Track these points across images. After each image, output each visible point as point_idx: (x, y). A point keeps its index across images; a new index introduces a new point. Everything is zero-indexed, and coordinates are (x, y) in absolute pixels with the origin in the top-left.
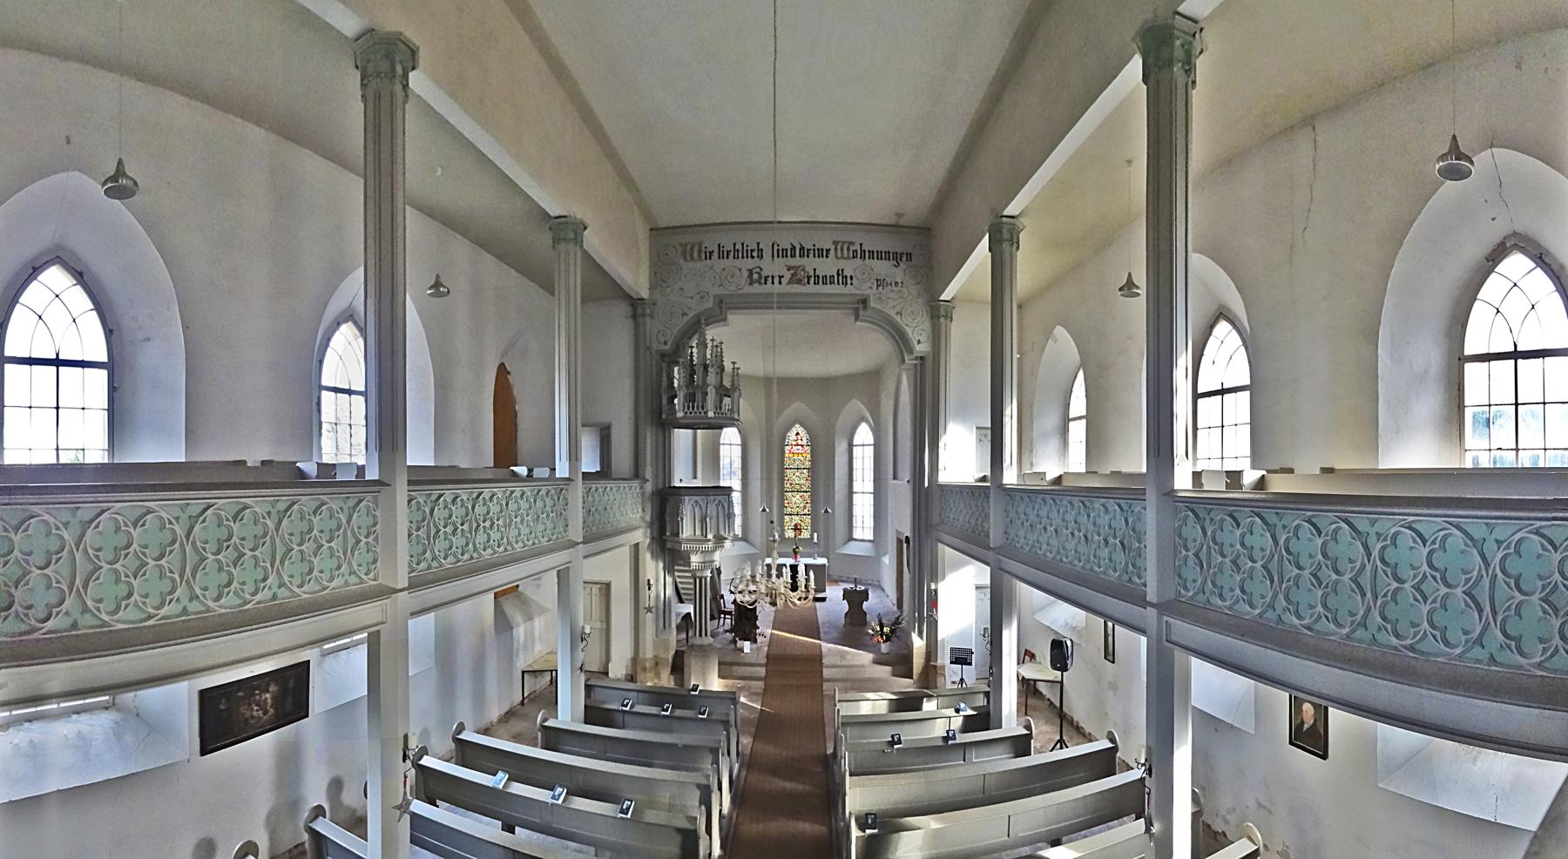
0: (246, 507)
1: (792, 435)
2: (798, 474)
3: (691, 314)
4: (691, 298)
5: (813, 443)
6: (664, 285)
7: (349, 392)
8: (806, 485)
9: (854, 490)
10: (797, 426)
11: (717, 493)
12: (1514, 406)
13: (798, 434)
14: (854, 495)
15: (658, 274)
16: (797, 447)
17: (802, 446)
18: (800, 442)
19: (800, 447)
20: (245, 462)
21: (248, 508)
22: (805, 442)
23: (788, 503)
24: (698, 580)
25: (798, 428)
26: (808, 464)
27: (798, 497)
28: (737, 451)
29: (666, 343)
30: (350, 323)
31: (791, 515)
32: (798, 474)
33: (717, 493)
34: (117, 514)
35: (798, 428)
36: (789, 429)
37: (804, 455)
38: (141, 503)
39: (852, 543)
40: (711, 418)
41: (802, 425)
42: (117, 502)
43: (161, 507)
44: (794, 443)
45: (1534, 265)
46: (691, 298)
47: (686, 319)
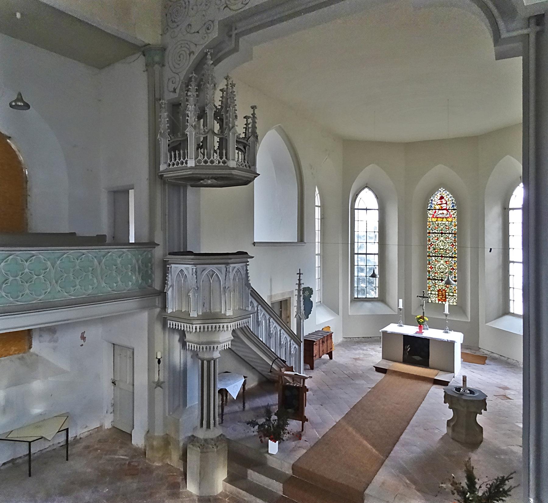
0: (124, 253)
1: (436, 199)
2: (442, 238)
3: (198, 51)
4: (198, 32)
5: (459, 207)
6: (175, 25)
7: (358, 209)
8: (453, 251)
9: (511, 259)
10: (441, 189)
11: (208, 261)
12: (365, 253)
13: (442, 198)
14: (511, 265)
15: (169, 15)
16: (441, 212)
17: (447, 210)
18: (444, 206)
19: (445, 212)
20: (75, 233)
21: (34, 256)
22: (450, 206)
23: (431, 268)
24: (205, 362)
25: (442, 192)
26: (454, 229)
27: (442, 262)
28: (373, 218)
29: (174, 91)
30: (366, 190)
31: (434, 279)
32: (442, 238)
33: (208, 261)
34: (17, 256)
35: (442, 192)
36: (432, 193)
37: (450, 220)
38: (120, 250)
39: (507, 317)
40: (191, 168)
41: (447, 188)
42: (72, 250)
43: (88, 252)
44: (437, 207)
45: (521, 261)
46: (198, 32)
47: (193, 57)
